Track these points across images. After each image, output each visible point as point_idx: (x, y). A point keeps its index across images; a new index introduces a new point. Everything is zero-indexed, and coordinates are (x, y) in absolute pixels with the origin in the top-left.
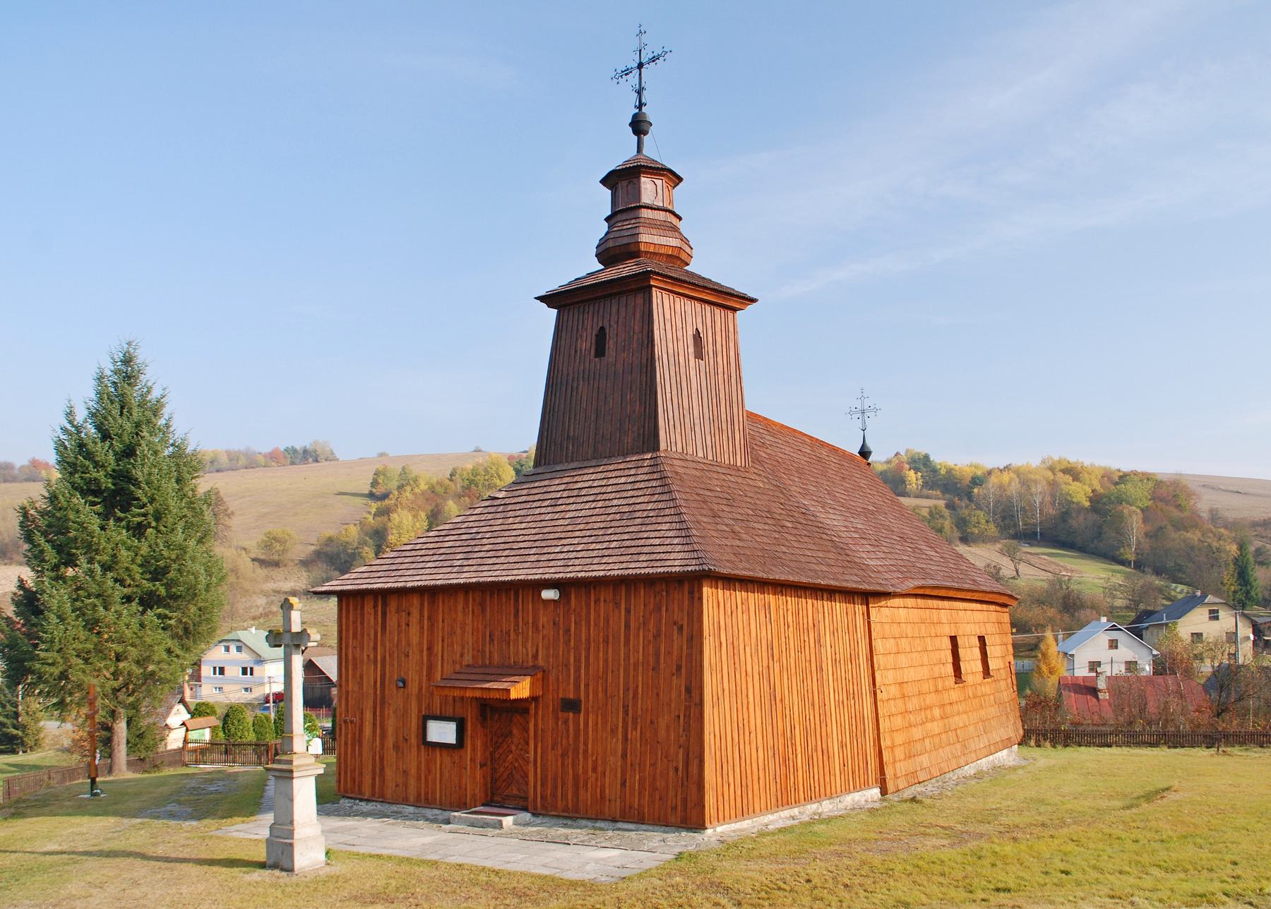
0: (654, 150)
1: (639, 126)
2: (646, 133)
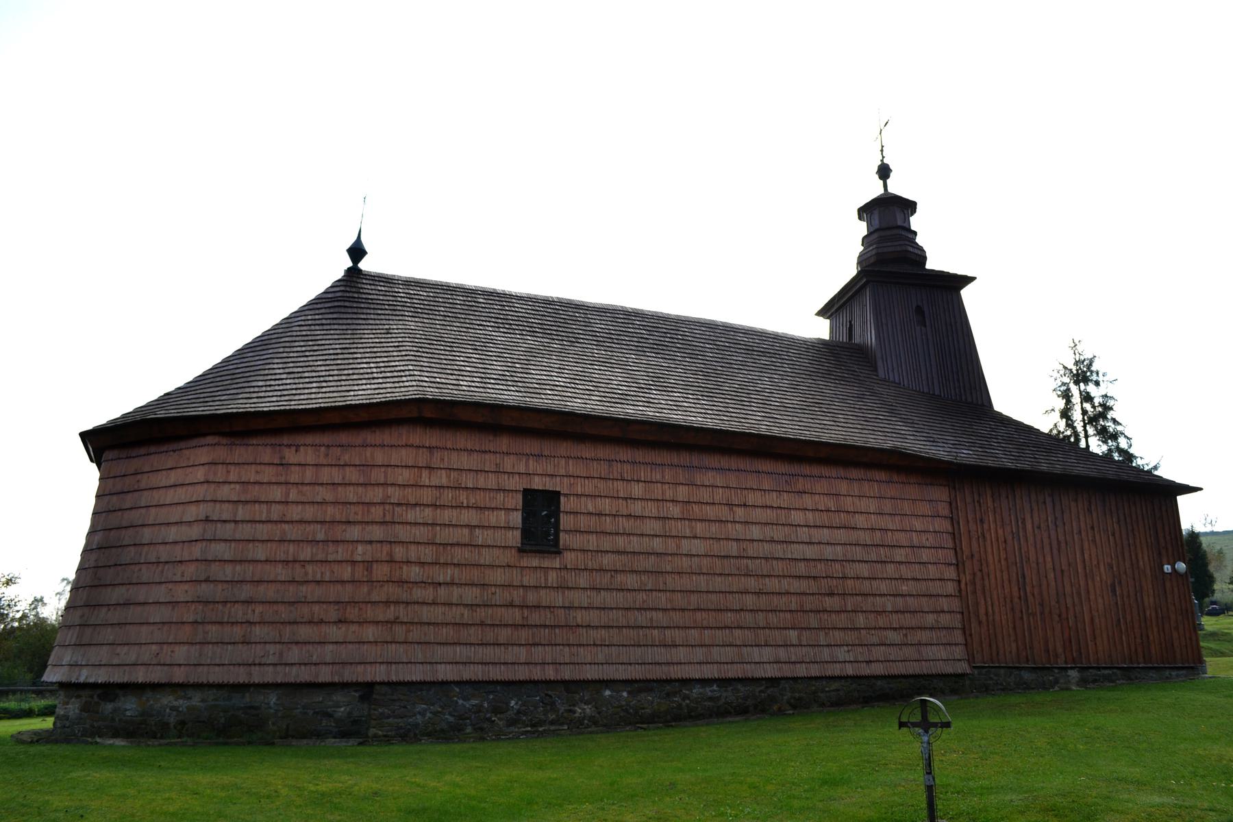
0: (897, 186)
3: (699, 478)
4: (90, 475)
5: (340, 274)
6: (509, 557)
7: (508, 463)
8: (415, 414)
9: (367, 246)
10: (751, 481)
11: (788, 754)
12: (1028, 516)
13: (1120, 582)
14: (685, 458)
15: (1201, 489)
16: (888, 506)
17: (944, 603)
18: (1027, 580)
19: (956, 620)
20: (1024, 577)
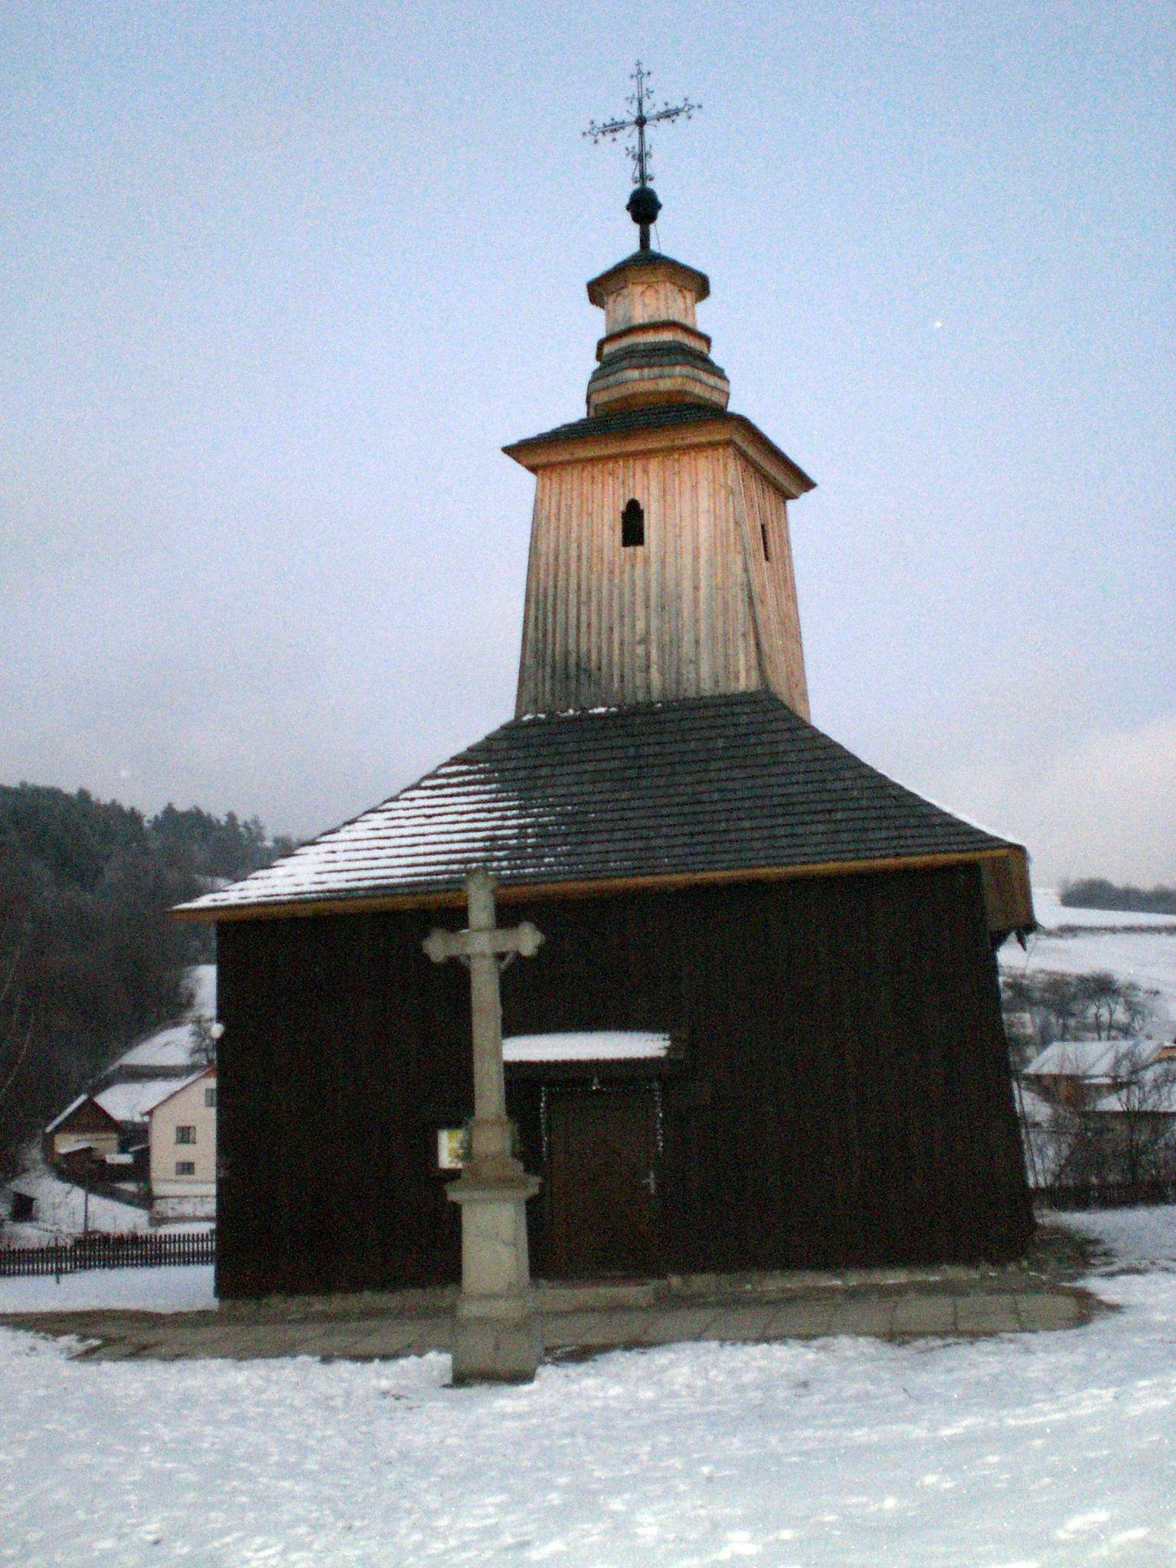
0: (668, 238)
1: (644, 207)
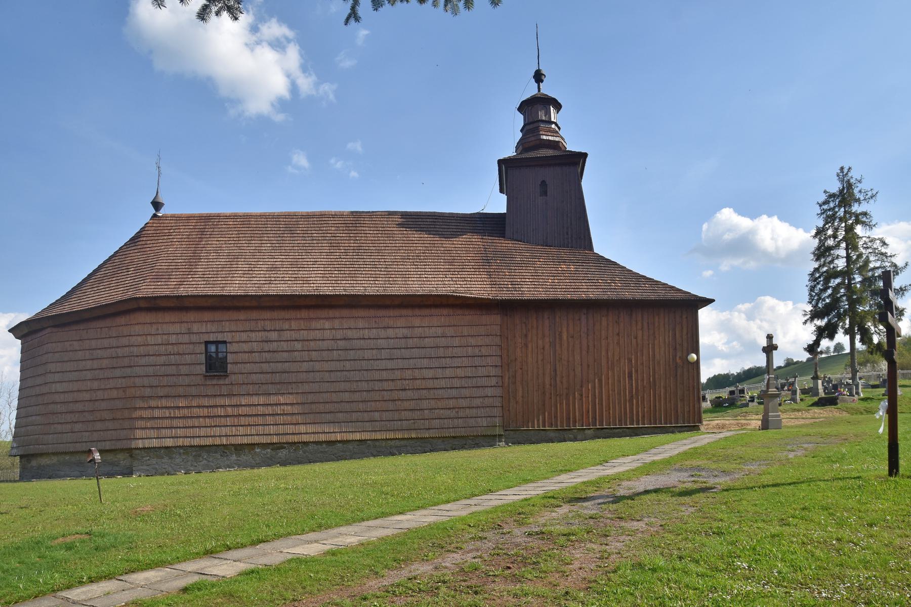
0: (547, 89)
1: (539, 77)
2: (542, 81)
3: (314, 324)
4: (17, 344)
5: (147, 219)
6: (199, 380)
7: (196, 328)
8: (136, 306)
9: (543, 72)
10: (352, 323)
11: (901, 429)
12: (565, 330)
13: (637, 371)
14: (304, 313)
15: (712, 301)
16: (450, 331)
17: (490, 392)
18: (558, 373)
19: (497, 402)
20: (556, 370)
